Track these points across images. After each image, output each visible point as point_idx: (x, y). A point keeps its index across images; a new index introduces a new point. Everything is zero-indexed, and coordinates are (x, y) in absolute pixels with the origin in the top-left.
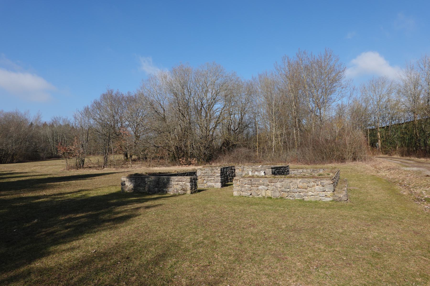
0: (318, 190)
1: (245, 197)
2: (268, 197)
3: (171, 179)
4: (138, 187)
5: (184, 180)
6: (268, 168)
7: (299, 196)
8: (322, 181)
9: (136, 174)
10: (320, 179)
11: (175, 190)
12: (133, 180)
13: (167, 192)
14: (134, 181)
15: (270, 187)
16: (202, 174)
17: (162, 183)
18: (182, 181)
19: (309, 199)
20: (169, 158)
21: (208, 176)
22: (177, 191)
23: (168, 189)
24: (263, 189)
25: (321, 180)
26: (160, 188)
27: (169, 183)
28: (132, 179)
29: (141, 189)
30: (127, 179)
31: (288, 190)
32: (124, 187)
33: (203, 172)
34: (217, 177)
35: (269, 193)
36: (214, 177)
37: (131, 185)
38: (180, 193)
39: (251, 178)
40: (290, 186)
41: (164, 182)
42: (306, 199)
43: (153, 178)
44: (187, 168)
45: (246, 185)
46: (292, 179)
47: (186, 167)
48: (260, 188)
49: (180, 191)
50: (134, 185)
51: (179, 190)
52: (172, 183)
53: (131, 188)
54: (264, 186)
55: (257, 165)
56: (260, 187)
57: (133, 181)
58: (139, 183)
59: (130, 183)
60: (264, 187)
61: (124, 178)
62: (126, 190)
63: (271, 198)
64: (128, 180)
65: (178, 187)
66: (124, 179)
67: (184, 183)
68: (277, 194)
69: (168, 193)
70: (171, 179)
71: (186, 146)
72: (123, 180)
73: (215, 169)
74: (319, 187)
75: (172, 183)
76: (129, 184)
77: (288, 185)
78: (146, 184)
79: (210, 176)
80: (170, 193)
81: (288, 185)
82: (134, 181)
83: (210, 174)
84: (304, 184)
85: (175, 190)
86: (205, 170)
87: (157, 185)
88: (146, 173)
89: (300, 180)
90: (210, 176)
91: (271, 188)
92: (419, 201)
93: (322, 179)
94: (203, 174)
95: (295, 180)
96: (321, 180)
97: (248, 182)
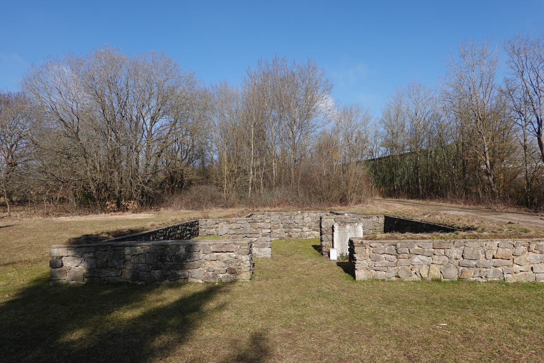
0: (532, 261)
1: (383, 280)
2: (433, 280)
3: (198, 248)
4: (103, 270)
5: (234, 250)
6: (364, 216)
7: (495, 273)
8: (538, 243)
9: (88, 238)
10: (536, 239)
11: (210, 273)
12: (88, 253)
13: (186, 278)
14: (91, 255)
15: (437, 259)
16: (230, 230)
17: (173, 258)
18: (227, 252)
19: (514, 278)
20: (76, 201)
21: (245, 235)
22: (215, 276)
23: (190, 271)
24: (422, 263)
25: (537, 241)
26: (169, 269)
27: (194, 257)
28: (83, 249)
29: (113, 274)
30: (69, 252)
31: (474, 263)
32: (59, 271)
33: (234, 226)
34: (263, 236)
35: (436, 272)
36: (257, 235)
37: (80, 267)
38: (224, 280)
39: (396, 241)
40: (478, 255)
41: (178, 255)
42: (511, 279)
43: (143, 247)
44: (122, 216)
45: (383, 256)
46: (483, 240)
47: (120, 214)
48: (415, 260)
49: (221, 276)
50: (91, 265)
51: (221, 272)
52: (201, 258)
53: (80, 274)
54: (424, 257)
55: (293, 211)
56: (416, 259)
57: (86, 255)
58: (107, 261)
59: (77, 261)
60: (424, 258)
61: (60, 250)
62: (66, 279)
63: (438, 281)
64: (70, 253)
65: (217, 266)
66: (58, 251)
67: (235, 255)
68: (453, 273)
69: (190, 280)
70: (198, 248)
71: (111, 181)
72: (55, 255)
73: (260, 221)
74: (535, 254)
75: (202, 255)
76: (76, 265)
77: (475, 253)
78: (125, 261)
79: (249, 235)
80: (195, 280)
81: (475, 253)
82: (91, 255)
83: (249, 231)
84: (506, 250)
85: (210, 273)
86: (238, 222)
87: (160, 263)
88: (108, 233)
89: (498, 242)
90: (249, 235)
91: (438, 261)
92: (108, 223)
93: (539, 239)
94: (232, 232)
95: (488, 243)
96: (537, 241)
97: (389, 250)
